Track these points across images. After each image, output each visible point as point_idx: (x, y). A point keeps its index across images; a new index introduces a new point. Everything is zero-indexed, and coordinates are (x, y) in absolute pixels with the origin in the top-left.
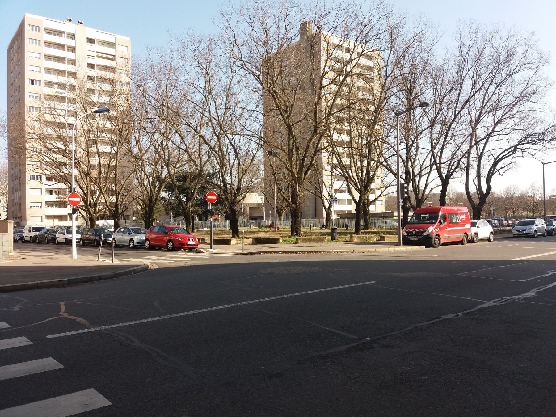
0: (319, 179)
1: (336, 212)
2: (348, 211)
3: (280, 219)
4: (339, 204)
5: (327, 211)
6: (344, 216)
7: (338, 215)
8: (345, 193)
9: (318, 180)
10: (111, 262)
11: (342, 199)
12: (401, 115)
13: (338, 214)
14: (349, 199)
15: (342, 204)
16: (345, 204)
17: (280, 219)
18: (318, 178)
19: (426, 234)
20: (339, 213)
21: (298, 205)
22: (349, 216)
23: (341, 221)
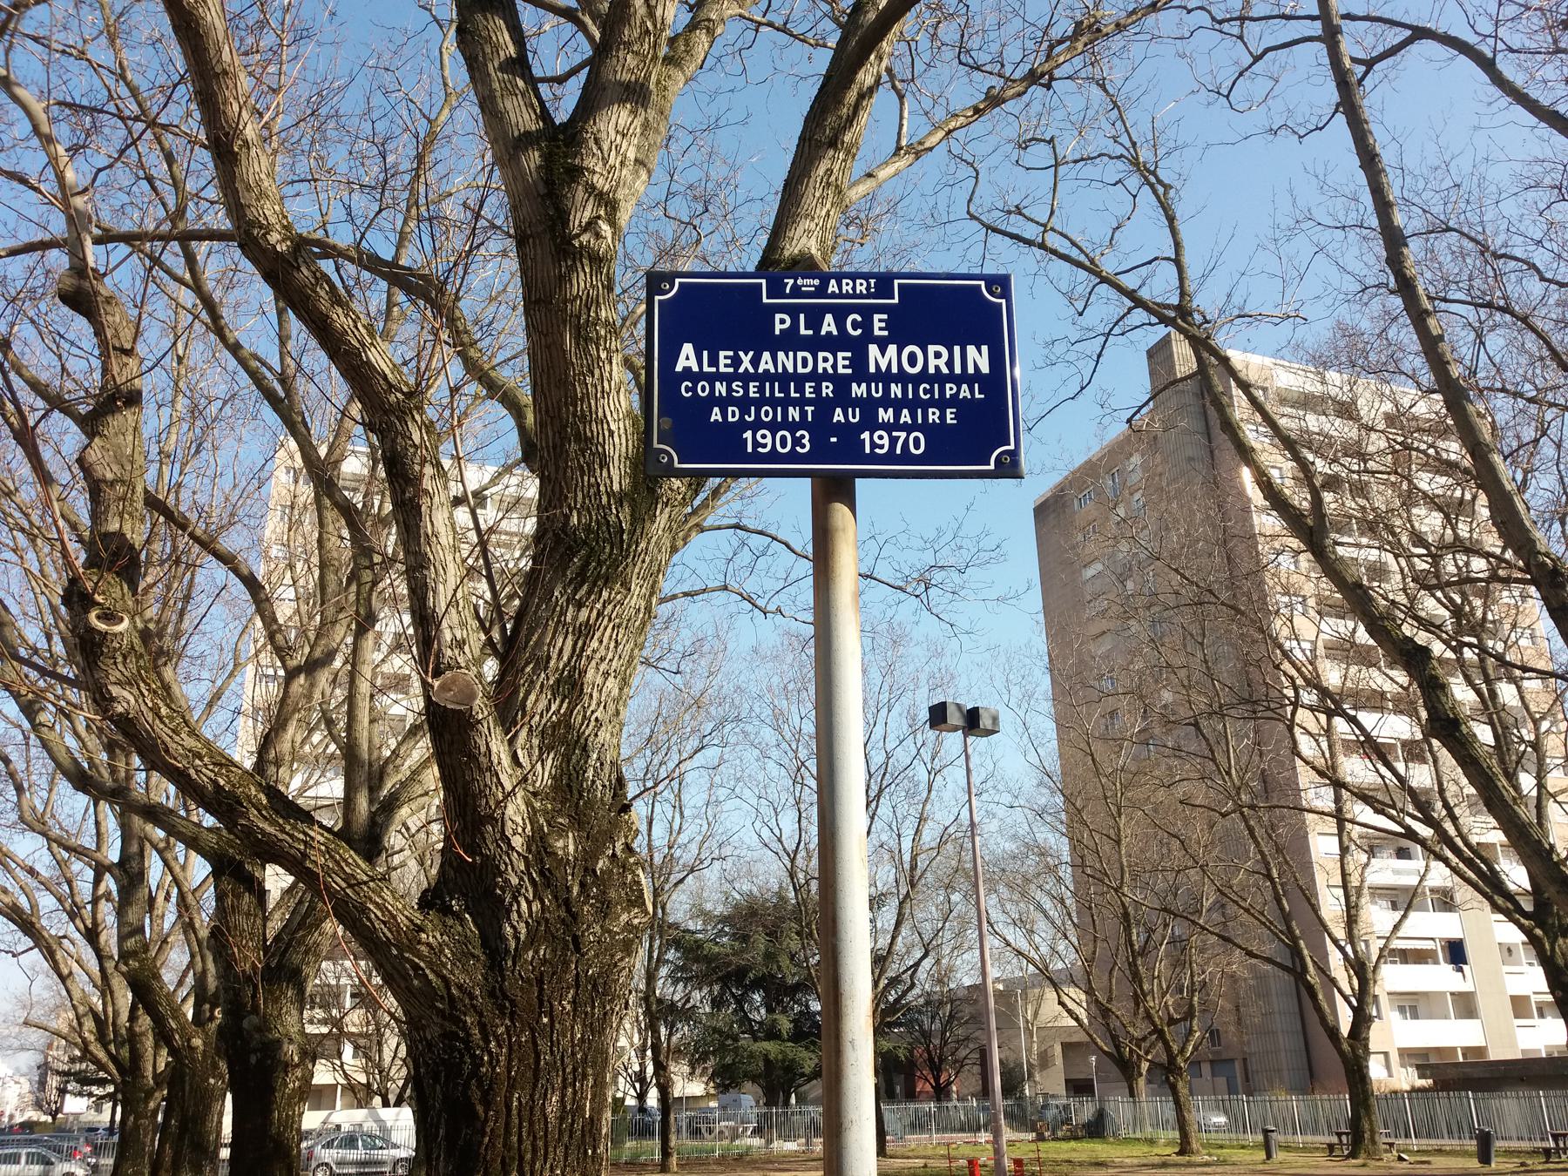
0: (1275, 874)
1: (1408, 1055)
2: (1467, 1051)
3: (1132, 1094)
4: (1415, 1016)
5: (1345, 1047)
6: (1452, 1074)
7: (1423, 1070)
8: (1436, 962)
9: (1269, 877)
10: (1262, 1155)
11: (1426, 994)
12: (1527, 524)
13: (1418, 1067)
14: (1460, 994)
15: (1431, 1017)
16: (1446, 1017)
17: (1132, 1094)
18: (1269, 870)
19: (528, 390)
20: (1422, 1060)
21: (515, 928)
22: (1477, 1073)
23: (1443, 1105)
